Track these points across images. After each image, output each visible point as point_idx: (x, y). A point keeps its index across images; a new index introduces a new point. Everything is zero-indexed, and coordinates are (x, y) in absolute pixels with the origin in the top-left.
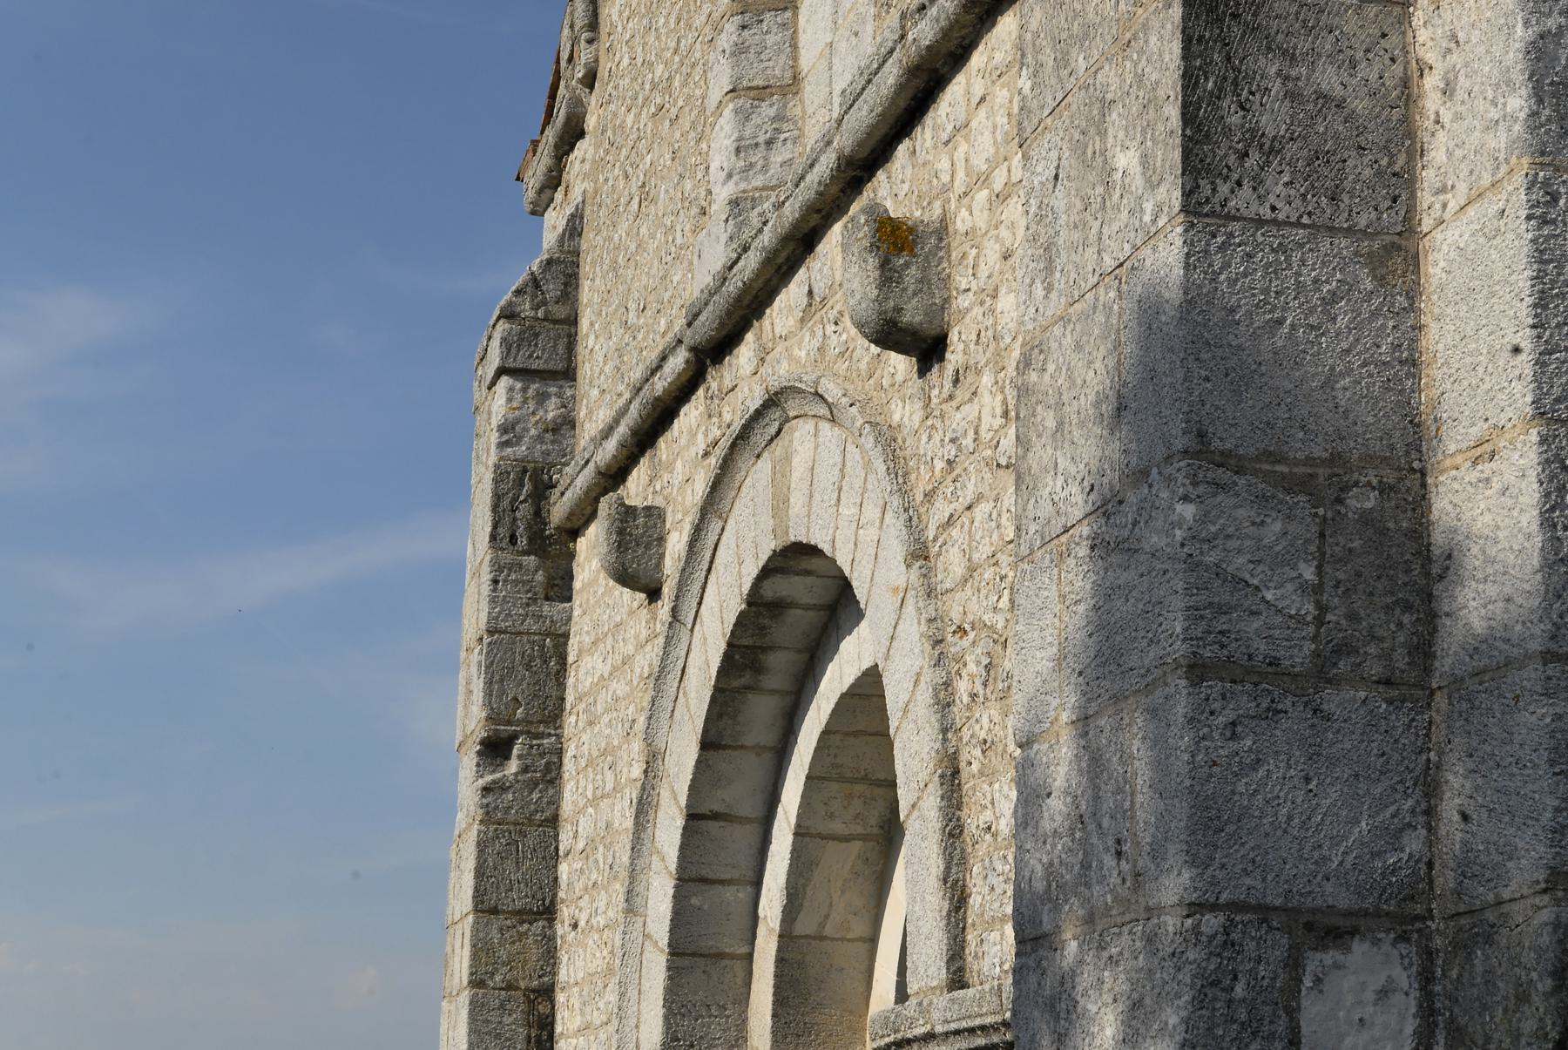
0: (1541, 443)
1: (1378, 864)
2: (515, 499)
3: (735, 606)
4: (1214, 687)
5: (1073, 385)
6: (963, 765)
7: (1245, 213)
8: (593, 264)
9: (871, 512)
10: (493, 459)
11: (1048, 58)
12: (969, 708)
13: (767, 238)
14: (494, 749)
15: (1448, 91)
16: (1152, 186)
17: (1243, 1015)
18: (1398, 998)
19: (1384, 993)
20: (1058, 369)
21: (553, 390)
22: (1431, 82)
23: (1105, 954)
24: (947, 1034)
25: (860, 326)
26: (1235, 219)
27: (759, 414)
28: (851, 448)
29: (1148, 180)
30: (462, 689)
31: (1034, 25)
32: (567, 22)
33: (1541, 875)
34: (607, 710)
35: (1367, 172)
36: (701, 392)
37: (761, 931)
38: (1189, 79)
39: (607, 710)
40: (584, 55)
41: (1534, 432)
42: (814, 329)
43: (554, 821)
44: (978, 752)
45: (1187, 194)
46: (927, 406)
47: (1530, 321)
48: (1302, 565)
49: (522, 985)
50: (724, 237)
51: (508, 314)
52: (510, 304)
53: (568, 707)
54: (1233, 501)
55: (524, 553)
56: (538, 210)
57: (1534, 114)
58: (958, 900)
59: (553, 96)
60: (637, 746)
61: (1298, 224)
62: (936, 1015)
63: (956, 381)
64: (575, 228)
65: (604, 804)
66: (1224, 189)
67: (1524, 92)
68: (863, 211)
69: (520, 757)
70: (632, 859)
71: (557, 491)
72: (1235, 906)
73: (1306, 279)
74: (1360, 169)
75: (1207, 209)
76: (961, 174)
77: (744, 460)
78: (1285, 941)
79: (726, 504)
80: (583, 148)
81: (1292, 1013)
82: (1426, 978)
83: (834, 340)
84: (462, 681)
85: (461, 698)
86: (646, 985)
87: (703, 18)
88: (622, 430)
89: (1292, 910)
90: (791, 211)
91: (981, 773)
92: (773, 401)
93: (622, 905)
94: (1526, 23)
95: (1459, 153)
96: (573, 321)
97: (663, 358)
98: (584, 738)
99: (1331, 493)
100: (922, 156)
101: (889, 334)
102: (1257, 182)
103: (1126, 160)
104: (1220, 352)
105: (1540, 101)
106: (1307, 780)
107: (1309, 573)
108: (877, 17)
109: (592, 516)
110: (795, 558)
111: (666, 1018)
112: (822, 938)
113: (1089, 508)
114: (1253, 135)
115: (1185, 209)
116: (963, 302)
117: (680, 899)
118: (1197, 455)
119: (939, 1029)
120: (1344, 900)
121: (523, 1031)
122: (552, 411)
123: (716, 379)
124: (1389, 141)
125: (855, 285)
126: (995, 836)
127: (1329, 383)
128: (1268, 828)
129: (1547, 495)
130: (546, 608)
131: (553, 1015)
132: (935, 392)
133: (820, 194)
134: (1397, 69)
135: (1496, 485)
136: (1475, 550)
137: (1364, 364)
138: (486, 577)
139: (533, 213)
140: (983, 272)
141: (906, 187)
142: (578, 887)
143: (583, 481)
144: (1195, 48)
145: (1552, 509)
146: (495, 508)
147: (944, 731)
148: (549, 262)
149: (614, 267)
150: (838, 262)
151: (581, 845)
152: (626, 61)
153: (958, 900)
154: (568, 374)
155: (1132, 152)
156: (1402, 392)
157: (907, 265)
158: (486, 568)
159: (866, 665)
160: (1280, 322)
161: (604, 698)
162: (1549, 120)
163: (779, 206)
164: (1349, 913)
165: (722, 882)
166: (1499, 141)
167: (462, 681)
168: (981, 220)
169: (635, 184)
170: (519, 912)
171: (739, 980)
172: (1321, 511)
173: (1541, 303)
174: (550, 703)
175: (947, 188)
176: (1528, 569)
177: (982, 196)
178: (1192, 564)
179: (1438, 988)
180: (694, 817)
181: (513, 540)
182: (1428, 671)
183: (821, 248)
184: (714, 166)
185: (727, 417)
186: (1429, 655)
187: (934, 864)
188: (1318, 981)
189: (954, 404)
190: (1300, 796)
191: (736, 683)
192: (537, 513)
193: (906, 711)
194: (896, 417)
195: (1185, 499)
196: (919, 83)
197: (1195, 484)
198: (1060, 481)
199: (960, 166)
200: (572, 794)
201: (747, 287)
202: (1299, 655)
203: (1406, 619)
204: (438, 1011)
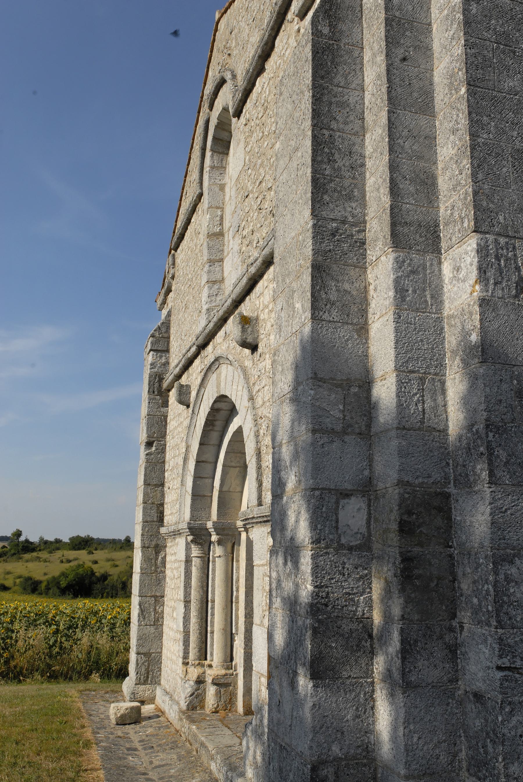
0: (396, 377)
1: (358, 478)
2: (154, 382)
3: (208, 410)
4: (318, 435)
5: (285, 360)
6: (261, 451)
7: (326, 319)
8: (174, 323)
9: (240, 388)
10: (149, 372)
11: (280, 279)
12: (263, 437)
13: (215, 319)
14: (149, 444)
15: (375, 290)
16: (304, 312)
17: (325, 515)
18: (363, 510)
19: (359, 509)
20: (282, 356)
21: (164, 355)
22: (372, 287)
23: (292, 500)
24: (257, 517)
25: (237, 342)
26: (324, 321)
27: (213, 363)
28: (235, 372)
29: (303, 311)
30: (141, 429)
31: (277, 271)
32: (167, 263)
33: (396, 481)
34: (177, 435)
35: (356, 309)
36: (199, 356)
37: (214, 490)
38: (313, 286)
39: (177, 435)
40: (172, 271)
41: (395, 374)
42: (226, 342)
43: (164, 462)
44: (265, 448)
45: (312, 315)
46: (253, 362)
47: (394, 347)
48: (340, 406)
49: (156, 503)
50: (205, 318)
51: (153, 336)
52: (153, 333)
53: (468, 148)
54: (323, 390)
55: (157, 395)
56: (160, 309)
57: (395, 296)
58: (260, 484)
59: (164, 281)
60: (184, 444)
61: (339, 322)
62: (255, 513)
63: (260, 356)
64: (169, 314)
65: (176, 458)
66: (321, 313)
67: (393, 291)
68: (238, 314)
69: (155, 446)
70: (183, 472)
71: (164, 380)
72: (323, 489)
73: (341, 335)
74: (354, 309)
75: (317, 318)
76: (261, 305)
77: (210, 374)
78: (335, 497)
79: (205, 385)
80: (171, 294)
81: (337, 514)
82: (369, 506)
83: (231, 345)
84: (141, 427)
85: (141, 431)
86: (186, 503)
87: (200, 263)
88: (180, 365)
89: (337, 490)
90: (221, 313)
91: (266, 453)
92: (217, 359)
93: (180, 484)
94: (394, 274)
95: (378, 305)
96: (169, 338)
97: (190, 348)
98: (171, 442)
99: (347, 388)
100: (252, 300)
101: (244, 344)
102: (329, 312)
103: (298, 306)
104: (320, 353)
105: (397, 293)
106: (341, 458)
107: (341, 407)
108: (242, 265)
109: (173, 387)
110: (222, 398)
111: (191, 511)
112: (230, 492)
113: (289, 391)
114: (328, 300)
115: (312, 318)
116: (262, 337)
117: (194, 482)
118: (314, 378)
119: (255, 516)
120: (349, 487)
121: (156, 515)
122: (163, 360)
123: (203, 353)
124: (361, 302)
125: (236, 332)
126: (269, 468)
127: (346, 361)
128: (331, 470)
129: (398, 389)
130: (162, 409)
131: (164, 510)
132: (255, 359)
133: (228, 309)
134: (363, 284)
135: (386, 386)
136: (381, 402)
137: (355, 356)
138: (147, 401)
139: (159, 310)
140: (267, 329)
141: (248, 308)
142: (170, 478)
143: (171, 378)
144: (314, 279)
145: (399, 392)
146: (149, 384)
147: (257, 442)
148: (163, 323)
149: (179, 325)
150: (232, 326)
151: (170, 468)
152: (182, 273)
153: (260, 484)
154: (167, 351)
155: (299, 304)
156: (364, 363)
157: (248, 327)
158: (147, 399)
159: (239, 425)
160: (335, 346)
161: (176, 432)
162: (399, 298)
163: (218, 311)
164: (350, 490)
165: (204, 478)
166: (387, 302)
167: (141, 427)
168: (266, 316)
169: (184, 304)
170: (155, 485)
171: (209, 502)
172: (344, 392)
173: (397, 343)
174: (163, 433)
175: (258, 308)
176: (393, 407)
177: (267, 310)
178: (313, 405)
179: (372, 508)
180: (198, 462)
181: (154, 392)
182: (370, 431)
183: (228, 322)
184: (203, 300)
185: (206, 363)
186: (370, 427)
187: (255, 475)
188: (343, 507)
189: (260, 362)
190: (339, 462)
191: (208, 429)
192: (160, 386)
193: (248, 437)
194: (246, 364)
195: (311, 389)
196: (251, 282)
197: (314, 386)
198: (283, 383)
199: (261, 303)
200: (169, 455)
201: (210, 331)
202: (339, 428)
203: (365, 418)
204: (135, 510)
